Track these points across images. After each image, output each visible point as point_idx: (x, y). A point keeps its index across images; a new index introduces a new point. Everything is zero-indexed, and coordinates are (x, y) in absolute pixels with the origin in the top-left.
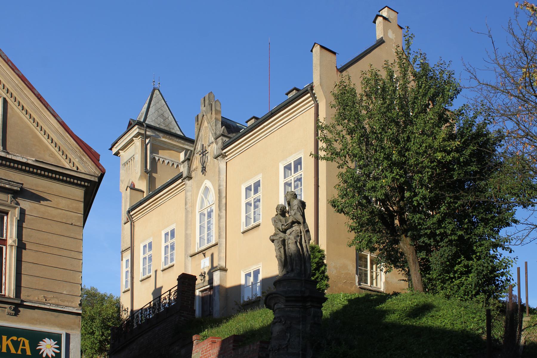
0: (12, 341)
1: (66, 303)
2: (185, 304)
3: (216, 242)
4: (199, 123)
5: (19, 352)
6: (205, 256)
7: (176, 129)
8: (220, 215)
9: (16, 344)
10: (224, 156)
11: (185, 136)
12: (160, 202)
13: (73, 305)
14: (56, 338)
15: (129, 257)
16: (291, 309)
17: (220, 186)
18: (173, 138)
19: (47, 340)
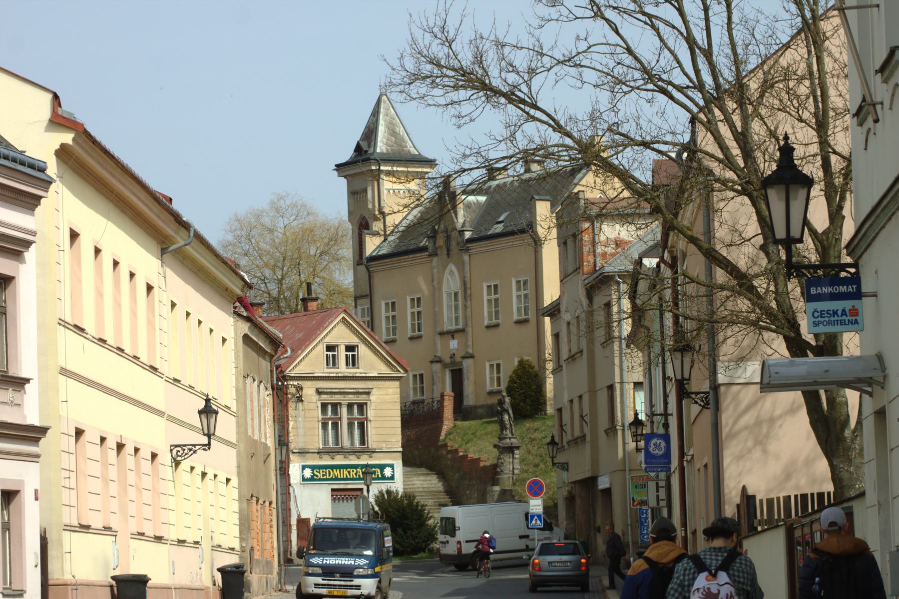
11: (419, 154)
14: (392, 466)
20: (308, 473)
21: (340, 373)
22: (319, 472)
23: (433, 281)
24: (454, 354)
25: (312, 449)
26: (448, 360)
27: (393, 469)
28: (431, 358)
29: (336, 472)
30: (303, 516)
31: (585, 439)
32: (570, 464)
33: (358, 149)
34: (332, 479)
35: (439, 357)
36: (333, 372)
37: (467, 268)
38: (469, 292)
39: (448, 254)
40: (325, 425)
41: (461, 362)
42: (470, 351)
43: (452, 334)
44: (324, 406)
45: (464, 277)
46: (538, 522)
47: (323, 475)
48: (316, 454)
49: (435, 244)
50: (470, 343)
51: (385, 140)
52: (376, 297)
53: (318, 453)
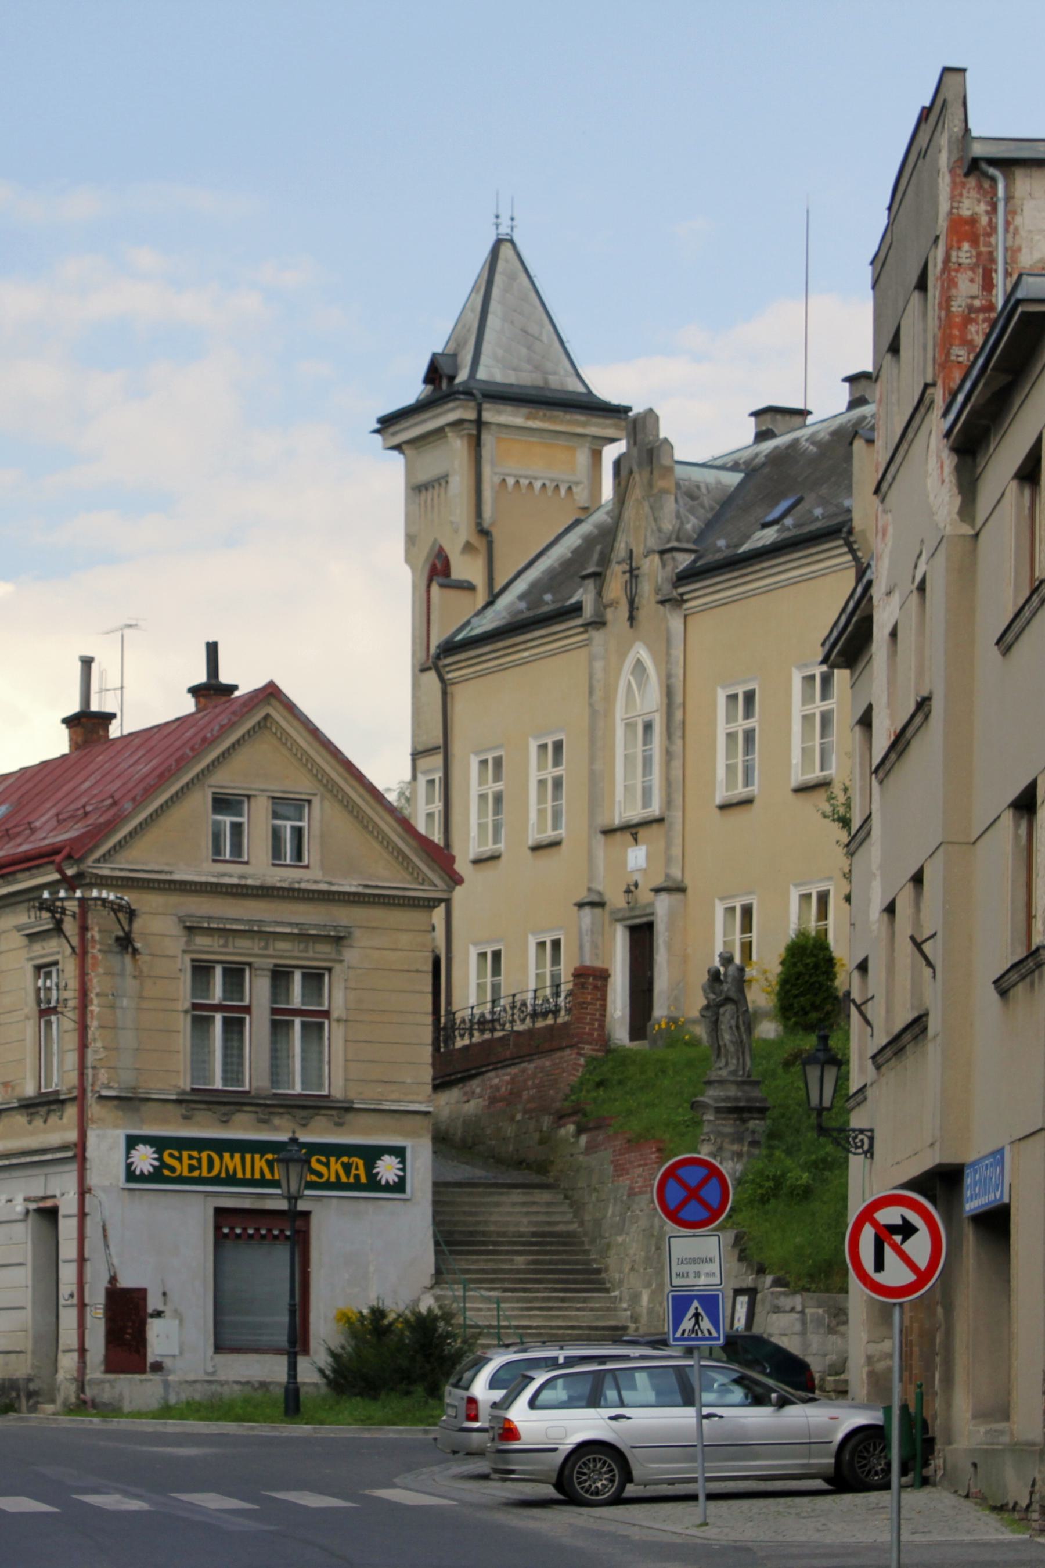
0: (343, 1164)
1: (410, 1098)
4: (623, 483)
5: (352, 1180)
6: (636, 840)
7: (562, 372)
9: (347, 1167)
10: (678, 602)
11: (590, 392)
12: (526, 654)
13: (420, 1098)
14: (399, 1152)
15: (438, 776)
16: (723, 1122)
17: (669, 676)
18: (559, 414)
19: (386, 1158)
20: (144, 1159)
21: (253, 876)
22: (180, 1159)
23: (591, 692)
24: (636, 885)
25: (161, 1091)
26: (617, 900)
27: (403, 1161)
28: (582, 895)
29: (232, 1162)
30: (126, 1282)
31: (925, 1029)
32: (877, 1135)
33: (435, 374)
34: (216, 1181)
35: (600, 894)
36: (231, 874)
37: (677, 652)
38: (678, 715)
39: (632, 618)
40: (201, 1022)
41: (652, 904)
42: (676, 873)
43: (633, 830)
44: (201, 971)
45: (669, 676)
46: (706, 1324)
47: (192, 1168)
48: (170, 1107)
49: (599, 594)
50: (677, 851)
51: (500, 352)
52: (457, 748)
53: (179, 1102)
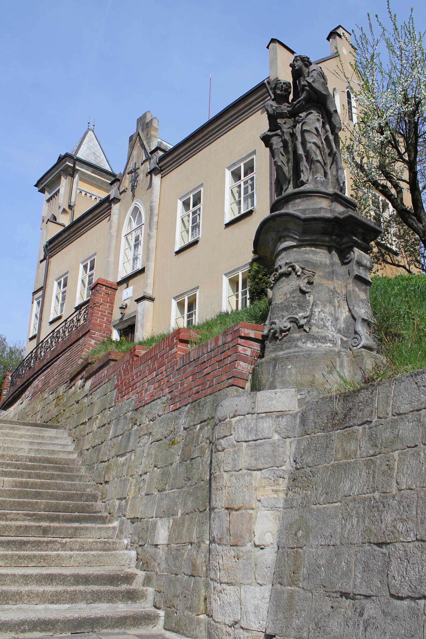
2: (98, 322)
3: (143, 267)
8: (150, 234)
